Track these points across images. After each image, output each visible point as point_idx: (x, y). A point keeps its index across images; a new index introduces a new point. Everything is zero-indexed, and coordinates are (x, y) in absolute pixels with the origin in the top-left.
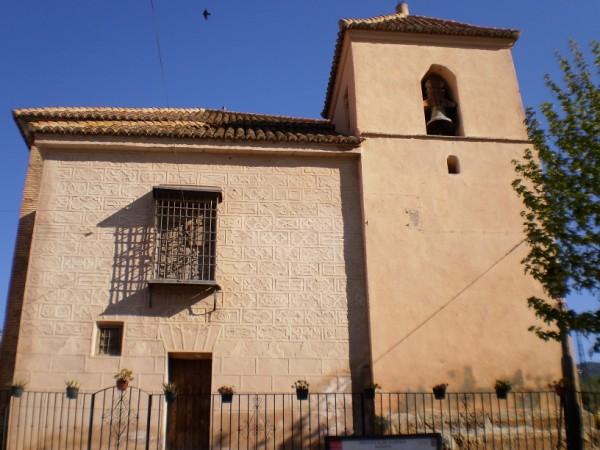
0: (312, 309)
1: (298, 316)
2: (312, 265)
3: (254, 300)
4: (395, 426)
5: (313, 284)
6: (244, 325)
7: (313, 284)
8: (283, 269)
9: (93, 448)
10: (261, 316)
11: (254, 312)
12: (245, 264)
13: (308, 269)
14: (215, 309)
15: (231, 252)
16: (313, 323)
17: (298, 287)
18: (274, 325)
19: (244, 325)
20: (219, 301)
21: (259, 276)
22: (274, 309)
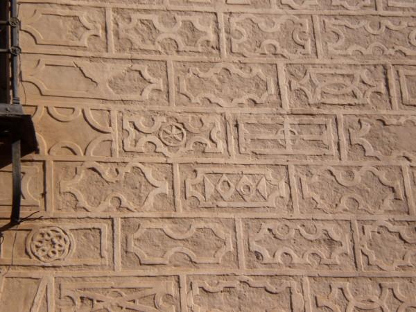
0: (383, 219)
1: (330, 242)
2: (364, 74)
3: (166, 189)
4: (107, 251)
5: (372, 136)
6: (132, 276)
7: (372, 136)
8: (260, 85)
9: (33, 310)
10: (195, 243)
11: (167, 227)
12: (122, 68)
13: (355, 86)
14: (15, 219)
15: (69, 25)
16: (392, 269)
17: (318, 143)
18: (244, 273)
19: (132, 276)
20: (29, 190)
21: (174, 108)
22: (239, 217)
